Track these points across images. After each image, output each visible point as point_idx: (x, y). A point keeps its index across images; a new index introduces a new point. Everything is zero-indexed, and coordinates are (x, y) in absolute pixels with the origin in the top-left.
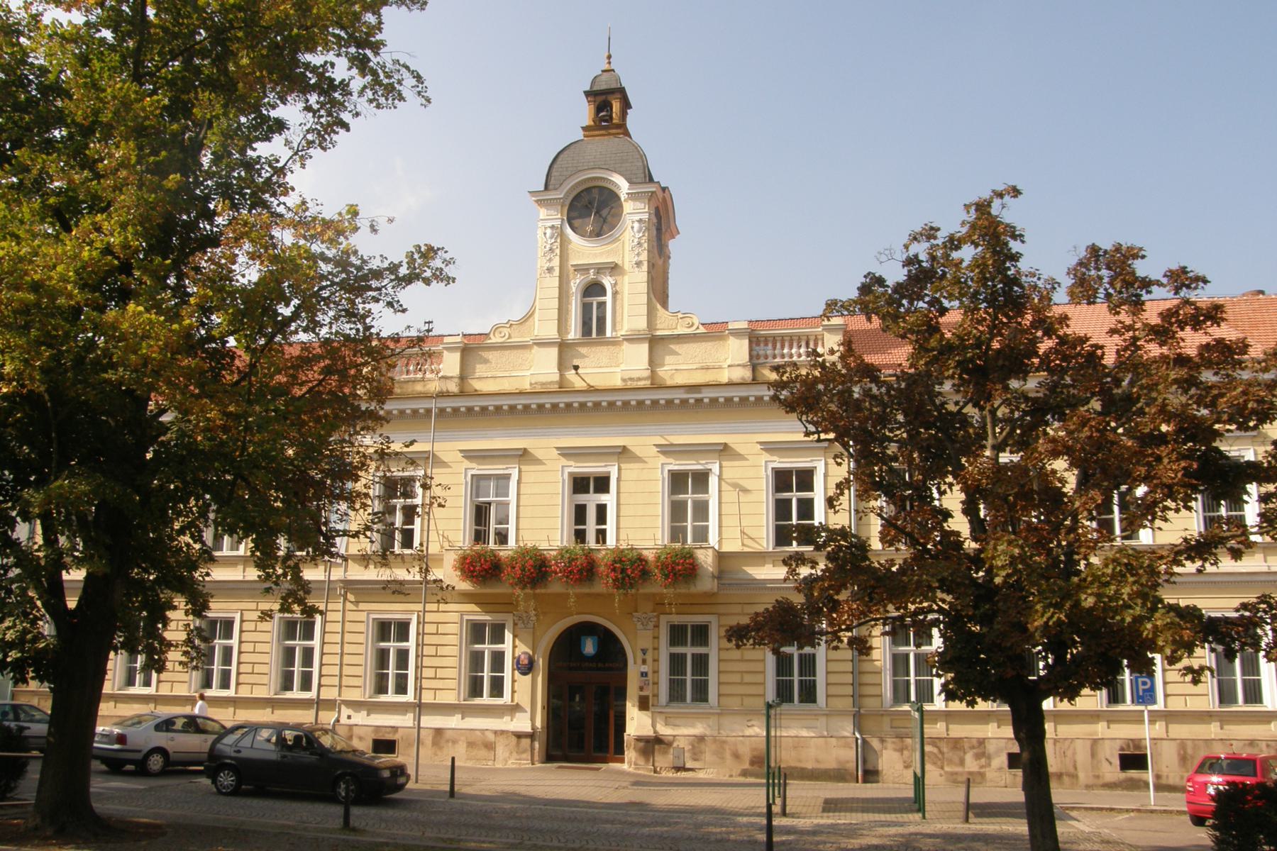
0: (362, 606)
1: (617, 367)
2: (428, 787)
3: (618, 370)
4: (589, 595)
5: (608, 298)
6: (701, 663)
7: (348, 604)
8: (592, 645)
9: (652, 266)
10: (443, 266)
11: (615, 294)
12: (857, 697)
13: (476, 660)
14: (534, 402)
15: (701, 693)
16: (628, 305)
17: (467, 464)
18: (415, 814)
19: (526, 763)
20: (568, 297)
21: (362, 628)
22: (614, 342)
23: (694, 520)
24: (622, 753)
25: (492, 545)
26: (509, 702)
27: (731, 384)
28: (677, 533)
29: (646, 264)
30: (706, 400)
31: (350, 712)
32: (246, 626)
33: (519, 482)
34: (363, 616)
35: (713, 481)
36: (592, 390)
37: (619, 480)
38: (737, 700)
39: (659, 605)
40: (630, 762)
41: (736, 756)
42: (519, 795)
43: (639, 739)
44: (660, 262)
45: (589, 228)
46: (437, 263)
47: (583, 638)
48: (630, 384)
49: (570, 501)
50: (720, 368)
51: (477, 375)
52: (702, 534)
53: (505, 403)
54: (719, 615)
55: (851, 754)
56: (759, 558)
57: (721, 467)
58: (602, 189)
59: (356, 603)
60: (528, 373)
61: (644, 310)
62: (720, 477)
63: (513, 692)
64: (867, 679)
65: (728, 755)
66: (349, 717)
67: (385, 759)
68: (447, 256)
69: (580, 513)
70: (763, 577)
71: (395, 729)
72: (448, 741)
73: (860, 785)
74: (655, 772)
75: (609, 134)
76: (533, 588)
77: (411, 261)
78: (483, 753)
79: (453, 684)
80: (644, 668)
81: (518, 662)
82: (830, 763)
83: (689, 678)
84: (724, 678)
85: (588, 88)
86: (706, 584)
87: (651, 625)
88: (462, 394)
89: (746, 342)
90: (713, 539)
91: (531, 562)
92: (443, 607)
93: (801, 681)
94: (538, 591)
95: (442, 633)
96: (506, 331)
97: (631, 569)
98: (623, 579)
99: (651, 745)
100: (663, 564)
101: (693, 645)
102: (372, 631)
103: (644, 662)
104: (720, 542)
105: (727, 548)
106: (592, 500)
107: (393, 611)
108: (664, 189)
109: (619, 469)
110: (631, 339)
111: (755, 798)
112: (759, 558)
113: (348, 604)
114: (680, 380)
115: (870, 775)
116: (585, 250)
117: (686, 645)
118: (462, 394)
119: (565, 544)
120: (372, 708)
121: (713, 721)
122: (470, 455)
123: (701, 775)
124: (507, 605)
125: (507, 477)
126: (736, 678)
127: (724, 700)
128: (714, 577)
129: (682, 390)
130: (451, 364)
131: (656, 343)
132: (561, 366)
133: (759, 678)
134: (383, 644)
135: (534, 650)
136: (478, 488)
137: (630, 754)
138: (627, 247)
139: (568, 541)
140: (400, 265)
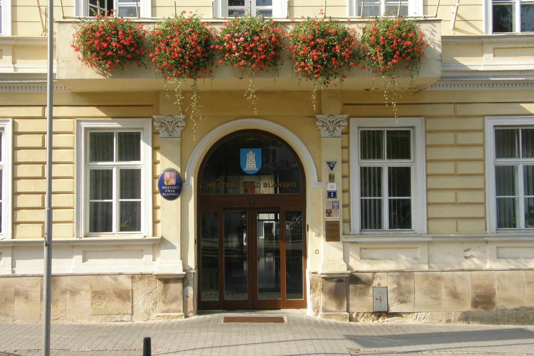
6: (401, 181)
13: (100, 182)
19: (178, 318)
26: (150, 236)
38: (451, 225)
41: (455, 295)
47: (242, 150)
54: (427, 117)
56: (475, 44)
63: (155, 222)
65: (443, 293)
72: (64, 292)
78: (116, 305)
80: (332, 187)
81: (161, 183)
87: (339, 130)
99: (343, 286)
103: (332, 178)
112: (475, 44)
121: (420, 252)
123: (409, 321)
126: (449, 197)
135: (183, 166)
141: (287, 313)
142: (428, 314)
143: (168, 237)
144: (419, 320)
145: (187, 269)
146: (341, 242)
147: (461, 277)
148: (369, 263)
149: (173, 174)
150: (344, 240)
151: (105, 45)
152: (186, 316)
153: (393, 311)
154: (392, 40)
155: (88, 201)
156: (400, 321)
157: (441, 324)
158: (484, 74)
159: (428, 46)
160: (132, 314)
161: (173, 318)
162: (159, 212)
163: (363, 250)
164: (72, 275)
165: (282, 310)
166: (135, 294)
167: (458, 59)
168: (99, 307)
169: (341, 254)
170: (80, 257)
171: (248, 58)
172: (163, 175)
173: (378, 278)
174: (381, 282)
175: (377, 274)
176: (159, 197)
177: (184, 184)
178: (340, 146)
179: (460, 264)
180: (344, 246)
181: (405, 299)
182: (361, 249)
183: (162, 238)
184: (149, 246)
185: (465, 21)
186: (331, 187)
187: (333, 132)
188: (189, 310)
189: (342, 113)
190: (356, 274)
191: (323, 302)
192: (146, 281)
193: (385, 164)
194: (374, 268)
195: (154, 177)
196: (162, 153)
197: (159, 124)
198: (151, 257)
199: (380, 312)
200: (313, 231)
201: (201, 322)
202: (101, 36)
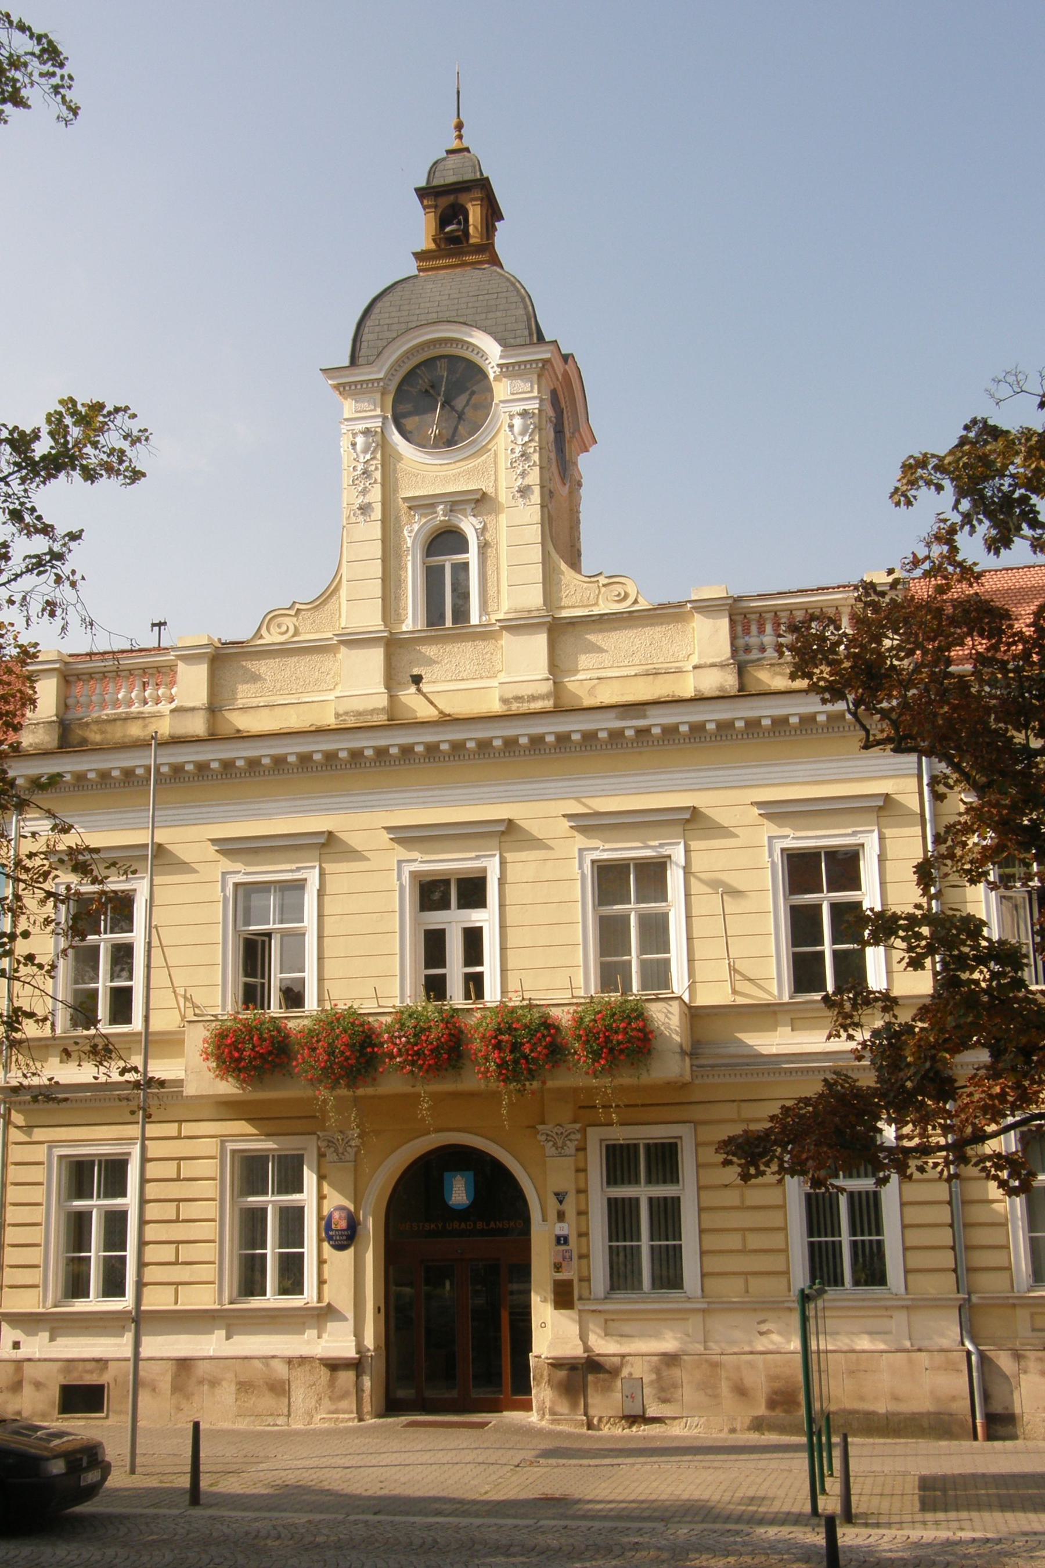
0: (39, 1134)
1: (491, 677)
2: (153, 1483)
3: (494, 683)
4: (455, 1095)
5: (472, 556)
6: (666, 1215)
7: (12, 1130)
8: (464, 1189)
9: (548, 495)
10: (125, 445)
11: (484, 547)
12: (963, 1272)
13: (252, 1224)
14: (342, 746)
15: (669, 1276)
16: (508, 567)
17: (226, 864)
18: (110, 1552)
19: (348, 1420)
20: (399, 556)
21: (37, 1174)
22: (485, 634)
23: (643, 949)
24: (528, 1391)
25: (275, 1010)
26: (314, 1303)
27: (699, 699)
28: (612, 975)
29: (537, 490)
30: (656, 731)
31: (17, 1335)
32: (153, 1170)
33: (321, 893)
34: (40, 1153)
35: (675, 879)
36: (447, 721)
37: (502, 882)
38: (738, 1283)
39: (586, 1110)
40: (543, 1410)
41: (741, 1391)
42: (329, 1492)
43: (557, 1364)
44: (564, 491)
45: (433, 431)
46: (112, 439)
47: (447, 1175)
48: (515, 707)
49: (416, 922)
50: (679, 671)
51: (240, 703)
52: (658, 975)
53: (291, 750)
54: (696, 1123)
55: (961, 1382)
56: (765, 1014)
57: (687, 851)
58: (453, 359)
59: (28, 1128)
60: (331, 696)
61: (537, 573)
62: (687, 871)
63: (321, 1282)
64: (981, 1237)
65: (725, 1388)
66: (16, 1345)
67: (81, 1427)
68: (134, 426)
69: (434, 945)
70: (774, 1050)
71: (102, 1363)
72: (201, 1382)
73: (980, 1444)
74: (590, 1426)
75: (464, 264)
76: (352, 1085)
77: (58, 430)
78: (268, 1401)
79: (208, 1272)
80: (562, 1229)
81: (328, 1227)
82: (920, 1403)
83: (645, 1243)
84: (712, 1242)
85: (423, 183)
86: (669, 1068)
87: (571, 1147)
88: (213, 737)
89: (724, 623)
90: (679, 983)
91: (345, 1038)
92: (188, 1129)
93: (854, 1244)
94: (360, 1092)
95: (184, 1184)
96: (289, 622)
97: (529, 1044)
98: (516, 1062)
99: (581, 1374)
100: (589, 1031)
101: (649, 1181)
102: (57, 1178)
103: (561, 1216)
104: (692, 988)
105: (705, 998)
106: (454, 921)
107: (97, 1140)
108: (566, 358)
109: (503, 863)
110: (517, 626)
111: (780, 1480)
112: (765, 1014)
113: (12, 1130)
114: (608, 695)
115: (1000, 1424)
116: (428, 471)
117: (637, 1182)
118: (213, 737)
119: (408, 1001)
120: (56, 1324)
121: (694, 1323)
122: (229, 848)
123: (676, 1430)
124: (302, 1120)
125: (299, 886)
126: (733, 1241)
127: (713, 1285)
128: (683, 1052)
129: (612, 714)
130: (192, 684)
131: (562, 632)
132: (391, 681)
133: (775, 1241)
134: (79, 1204)
135: (357, 1202)
136: (247, 910)
137: (542, 1394)
138: (503, 463)
139: (415, 996)
140: (36, 436)
141: (514, 1416)
142: (703, 1420)
143: (338, 1305)
144: (690, 1427)
145: (364, 1350)
146: (576, 1310)
147: (749, 1362)
148: (618, 1342)
149: (344, 1214)
150: (580, 1307)
151: (236, 1055)
152: (361, 1420)
153: (651, 1415)
154: (598, 1033)
155: (236, 1252)
156: (662, 1430)
157: (722, 1435)
158: (773, 1059)
159: (662, 1034)
160: (289, 1415)
161: (342, 1422)
162: (326, 1267)
163: (610, 1323)
164: (211, 1358)
165: (505, 1413)
166: (293, 1387)
167: (739, 1035)
168: (246, 1405)
169: (575, 1329)
170: (223, 1333)
171: (413, 1063)
172: (330, 1215)
173: (629, 1366)
174: (632, 1370)
175: (627, 1358)
176: (326, 1245)
177: (359, 1227)
178: (573, 1168)
179: (750, 1343)
180: (580, 1317)
181: (669, 1396)
182: (606, 1321)
183: (329, 1304)
184: (313, 1316)
185: (749, 980)
186: (561, 1229)
187: (562, 1148)
188: (365, 1410)
189: (575, 1122)
190: (596, 1358)
191: (551, 1401)
192: (307, 1368)
193: (643, 1192)
194: (624, 1349)
195: (320, 1218)
196: (329, 1185)
197: (325, 1144)
198: (315, 1331)
199: (634, 1416)
200: (537, 1293)
201: (381, 1426)
202: (232, 1043)
